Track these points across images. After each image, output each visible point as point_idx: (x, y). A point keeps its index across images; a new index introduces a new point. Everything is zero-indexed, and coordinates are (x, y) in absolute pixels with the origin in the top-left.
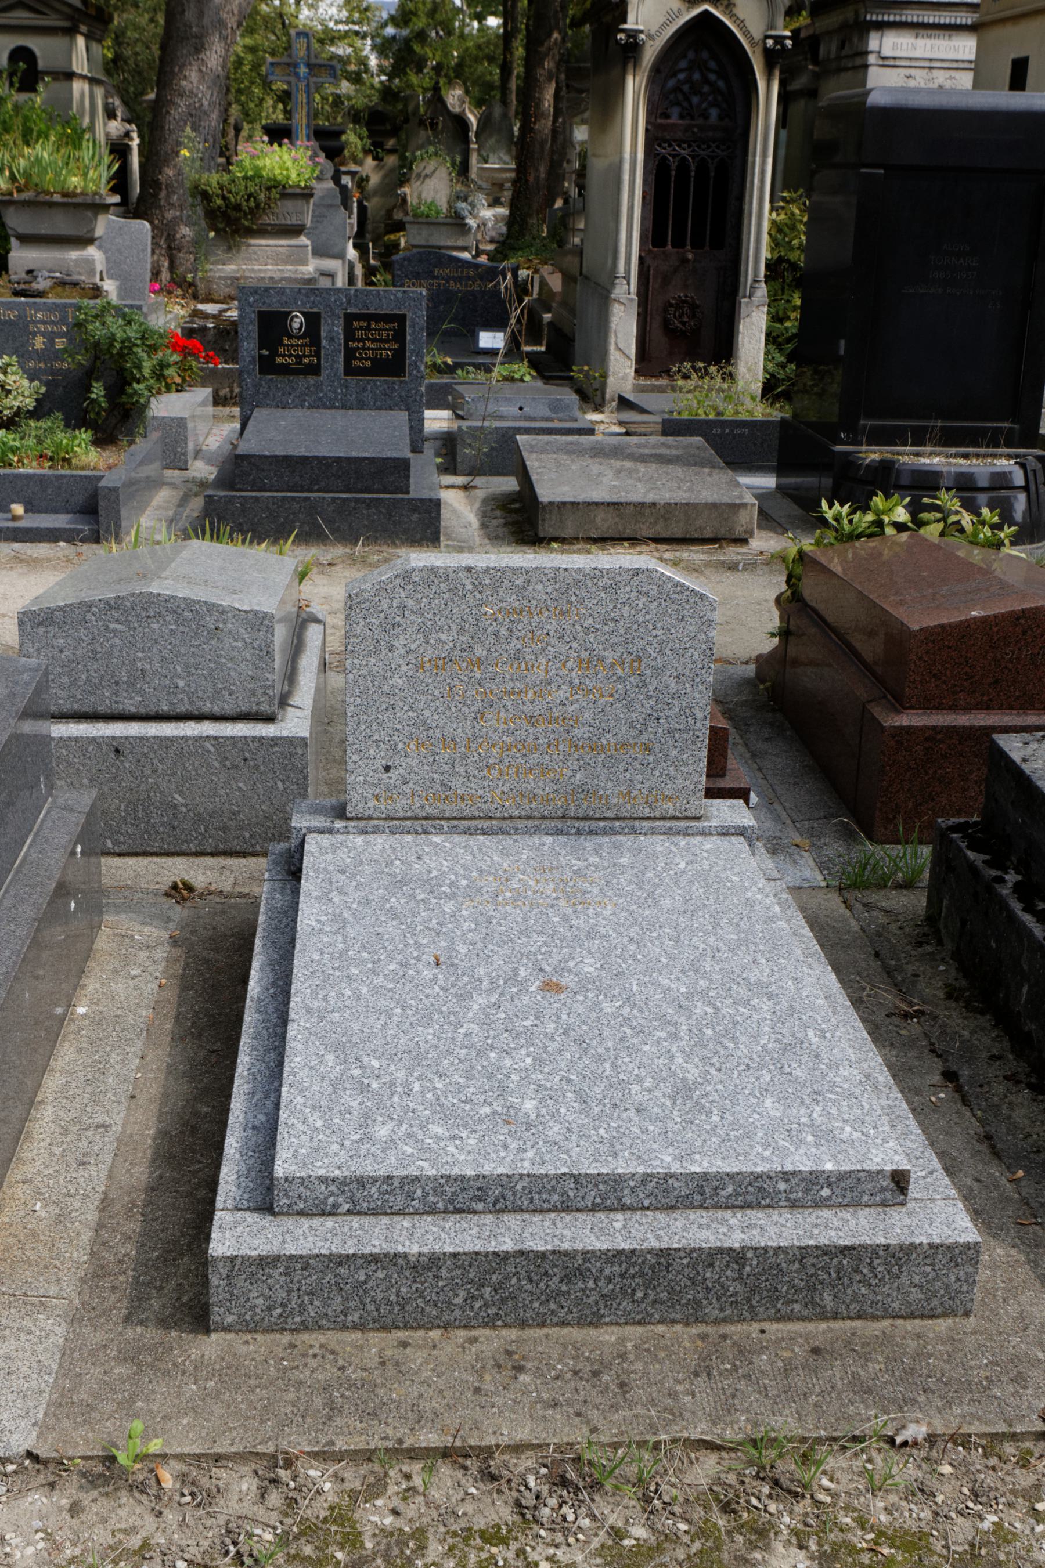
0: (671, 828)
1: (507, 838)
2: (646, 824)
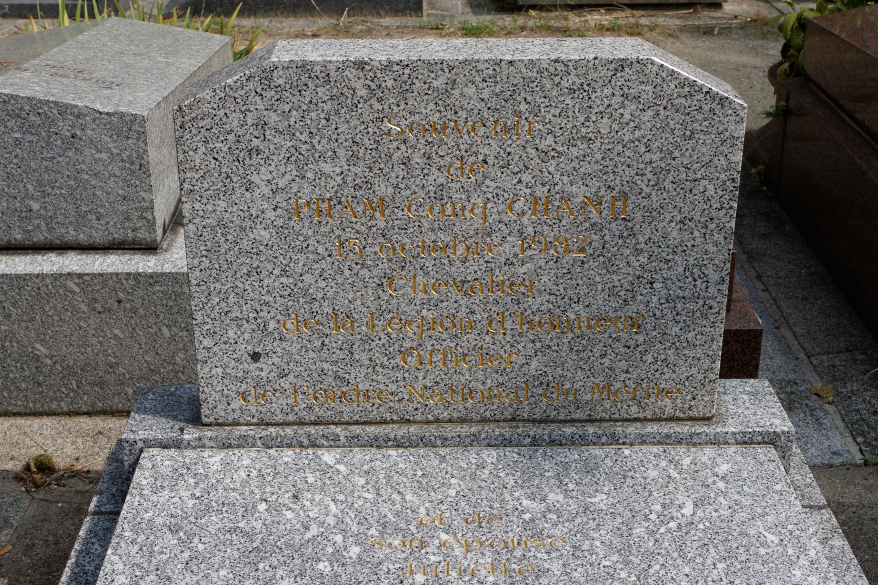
0: (668, 436)
1: (431, 452)
2: (632, 429)
